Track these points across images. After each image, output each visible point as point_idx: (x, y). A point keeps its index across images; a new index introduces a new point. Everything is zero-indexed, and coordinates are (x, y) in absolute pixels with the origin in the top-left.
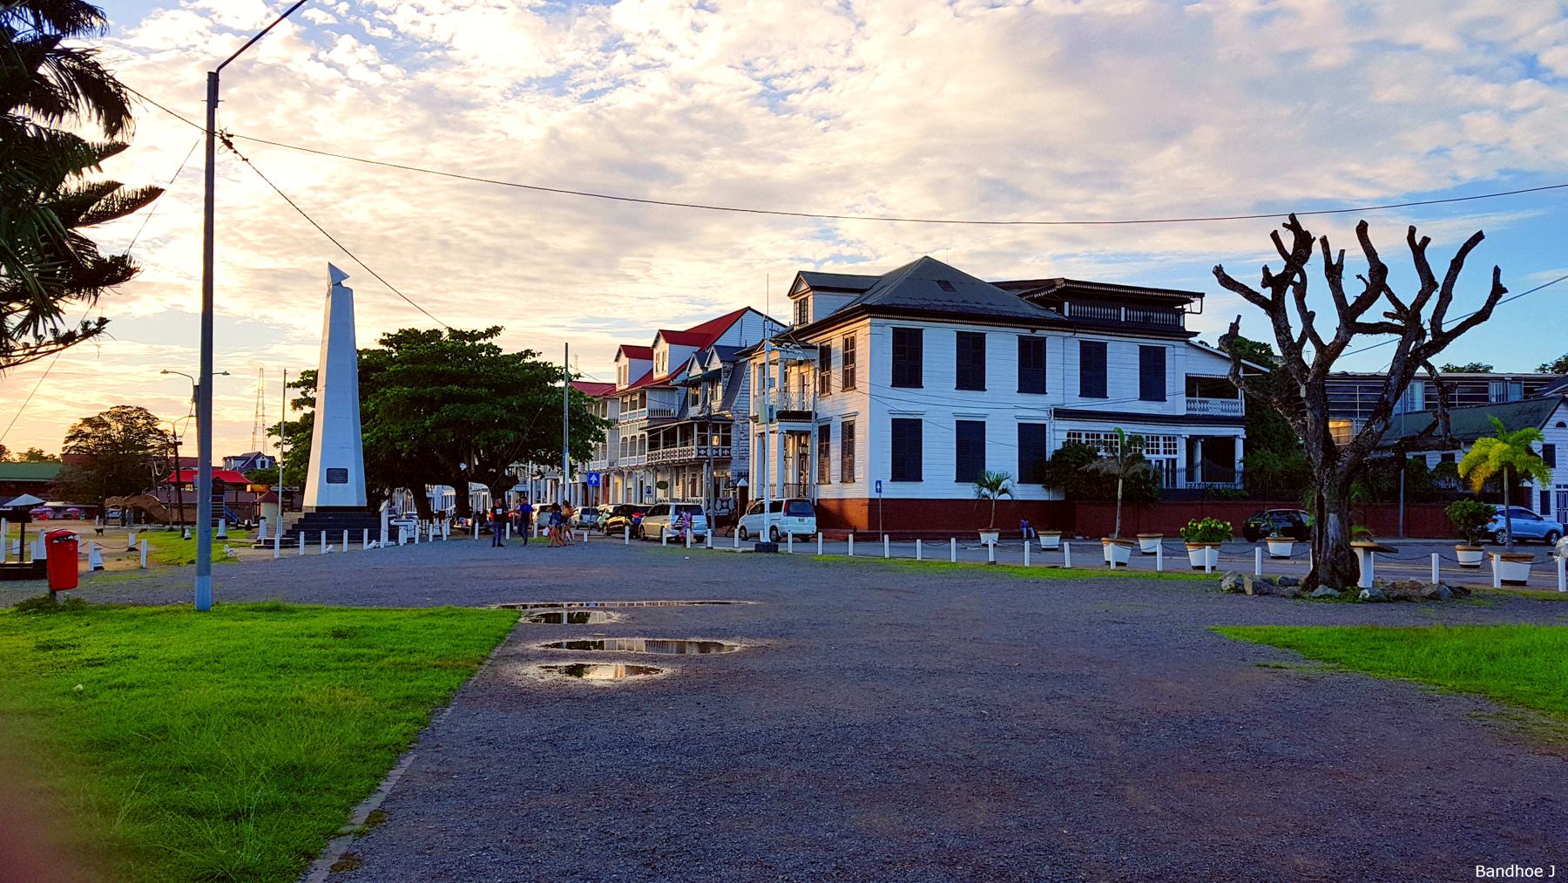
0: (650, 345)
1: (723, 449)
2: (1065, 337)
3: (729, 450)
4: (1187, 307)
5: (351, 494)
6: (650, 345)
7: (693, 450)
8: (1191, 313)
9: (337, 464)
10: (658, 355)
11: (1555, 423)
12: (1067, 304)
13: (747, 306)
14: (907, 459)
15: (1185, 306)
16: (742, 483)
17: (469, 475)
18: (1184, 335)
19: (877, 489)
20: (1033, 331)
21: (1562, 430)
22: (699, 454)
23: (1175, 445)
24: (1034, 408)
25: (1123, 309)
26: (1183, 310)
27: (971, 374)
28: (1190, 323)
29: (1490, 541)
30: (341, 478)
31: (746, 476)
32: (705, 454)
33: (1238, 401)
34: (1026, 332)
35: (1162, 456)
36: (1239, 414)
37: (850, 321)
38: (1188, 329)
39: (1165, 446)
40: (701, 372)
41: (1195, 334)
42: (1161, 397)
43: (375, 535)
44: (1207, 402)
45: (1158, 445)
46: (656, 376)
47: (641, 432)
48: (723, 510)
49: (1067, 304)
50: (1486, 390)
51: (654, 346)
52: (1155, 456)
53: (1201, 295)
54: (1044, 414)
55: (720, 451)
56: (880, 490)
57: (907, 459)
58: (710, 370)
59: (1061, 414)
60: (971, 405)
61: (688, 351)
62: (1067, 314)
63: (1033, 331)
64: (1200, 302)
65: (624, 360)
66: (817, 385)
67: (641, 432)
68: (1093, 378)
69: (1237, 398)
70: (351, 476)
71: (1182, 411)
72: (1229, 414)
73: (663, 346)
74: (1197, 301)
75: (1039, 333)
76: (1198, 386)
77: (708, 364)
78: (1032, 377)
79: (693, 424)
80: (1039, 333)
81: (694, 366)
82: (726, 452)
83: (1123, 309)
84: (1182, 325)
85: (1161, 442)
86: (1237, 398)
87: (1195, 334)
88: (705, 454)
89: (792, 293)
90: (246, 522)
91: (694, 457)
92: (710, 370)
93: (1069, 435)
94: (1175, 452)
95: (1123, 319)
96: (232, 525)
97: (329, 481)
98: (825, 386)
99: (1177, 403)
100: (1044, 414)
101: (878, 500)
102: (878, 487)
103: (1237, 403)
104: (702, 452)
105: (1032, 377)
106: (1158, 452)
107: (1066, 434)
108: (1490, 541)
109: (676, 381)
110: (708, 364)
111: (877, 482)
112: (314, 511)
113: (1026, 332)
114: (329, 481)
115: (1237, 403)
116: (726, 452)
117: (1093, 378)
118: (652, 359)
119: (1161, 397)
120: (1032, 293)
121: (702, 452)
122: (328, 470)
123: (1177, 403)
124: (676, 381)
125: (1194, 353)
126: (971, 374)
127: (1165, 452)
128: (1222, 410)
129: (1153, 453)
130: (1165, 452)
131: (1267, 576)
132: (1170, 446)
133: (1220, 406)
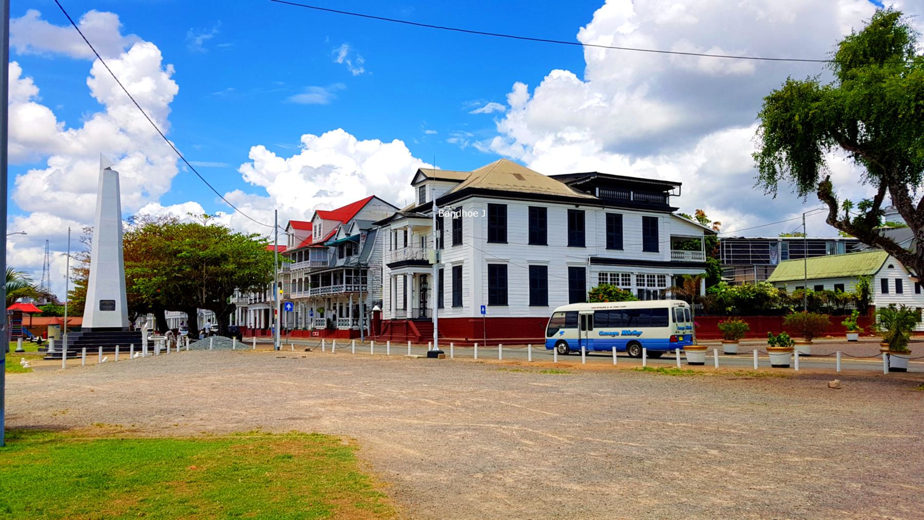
0: (310, 221)
1: (355, 287)
2: (596, 211)
3: (366, 287)
4: (670, 192)
5: (116, 319)
6: (310, 221)
7: (342, 287)
8: (674, 195)
9: (107, 297)
10: (315, 227)
11: (888, 265)
12: (597, 189)
13: (372, 195)
14: (498, 294)
15: (669, 191)
16: (376, 308)
17: (201, 304)
18: (670, 210)
19: (482, 311)
20: (577, 206)
21: (891, 270)
22: (347, 290)
23: (629, 280)
24: (579, 257)
25: (632, 193)
26: (668, 193)
27: (538, 236)
28: (672, 202)
29: (231, 315)
30: (111, 307)
31: (380, 304)
32: (351, 290)
33: (702, 252)
34: (573, 207)
35: (657, 288)
36: (702, 261)
37: (464, 198)
38: (671, 205)
39: (623, 280)
40: (345, 237)
41: (676, 209)
42: (656, 249)
43: (138, 348)
44: (683, 253)
45: (618, 280)
46: (314, 241)
47: (306, 276)
48: (354, 327)
49: (597, 189)
50: (824, 247)
51: (312, 221)
52: (653, 288)
53: (680, 184)
54: (584, 261)
55: (353, 287)
56: (485, 311)
57: (498, 294)
58: (352, 235)
59: (595, 261)
60: (538, 255)
61: (332, 225)
62: (597, 195)
63: (577, 206)
64: (679, 189)
65: (292, 231)
66: (392, 246)
67: (306, 276)
68: (615, 239)
69: (701, 250)
70: (118, 306)
71: (668, 259)
72: (697, 261)
73: (318, 222)
74: (677, 189)
75: (581, 208)
76: (678, 243)
77: (351, 231)
78: (577, 238)
79: (343, 270)
80: (581, 208)
81: (341, 233)
82: (356, 288)
83: (632, 193)
84: (667, 203)
85: (620, 278)
86: (701, 250)
87: (676, 209)
88: (351, 290)
89: (414, 183)
90: (38, 338)
91: (343, 291)
92: (352, 235)
93: (600, 274)
94: (629, 284)
95: (632, 199)
96: (28, 340)
97: (102, 309)
98: (441, 244)
99: (665, 253)
100: (584, 261)
101: (482, 318)
102: (483, 310)
103: (700, 254)
104: (349, 288)
105: (577, 238)
106: (654, 286)
107: (598, 274)
108: (231, 315)
109: (329, 243)
110: (351, 231)
111: (482, 307)
112: (90, 332)
113: (573, 207)
114: (102, 309)
115: (700, 254)
116: (356, 288)
117: (615, 239)
118: (312, 230)
119: (656, 249)
120: (575, 181)
121: (349, 288)
122: (101, 301)
123: (665, 253)
124: (329, 243)
125: (673, 221)
126: (538, 236)
127: (659, 286)
128: (693, 258)
129: (651, 286)
130: (623, 284)
131: (493, 348)
132: (626, 280)
133: (684, 255)
